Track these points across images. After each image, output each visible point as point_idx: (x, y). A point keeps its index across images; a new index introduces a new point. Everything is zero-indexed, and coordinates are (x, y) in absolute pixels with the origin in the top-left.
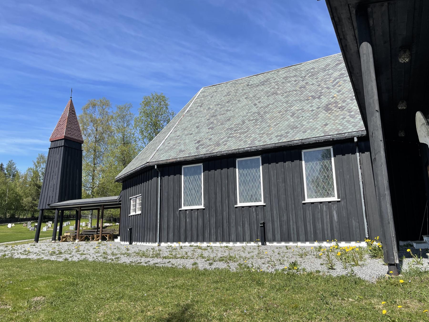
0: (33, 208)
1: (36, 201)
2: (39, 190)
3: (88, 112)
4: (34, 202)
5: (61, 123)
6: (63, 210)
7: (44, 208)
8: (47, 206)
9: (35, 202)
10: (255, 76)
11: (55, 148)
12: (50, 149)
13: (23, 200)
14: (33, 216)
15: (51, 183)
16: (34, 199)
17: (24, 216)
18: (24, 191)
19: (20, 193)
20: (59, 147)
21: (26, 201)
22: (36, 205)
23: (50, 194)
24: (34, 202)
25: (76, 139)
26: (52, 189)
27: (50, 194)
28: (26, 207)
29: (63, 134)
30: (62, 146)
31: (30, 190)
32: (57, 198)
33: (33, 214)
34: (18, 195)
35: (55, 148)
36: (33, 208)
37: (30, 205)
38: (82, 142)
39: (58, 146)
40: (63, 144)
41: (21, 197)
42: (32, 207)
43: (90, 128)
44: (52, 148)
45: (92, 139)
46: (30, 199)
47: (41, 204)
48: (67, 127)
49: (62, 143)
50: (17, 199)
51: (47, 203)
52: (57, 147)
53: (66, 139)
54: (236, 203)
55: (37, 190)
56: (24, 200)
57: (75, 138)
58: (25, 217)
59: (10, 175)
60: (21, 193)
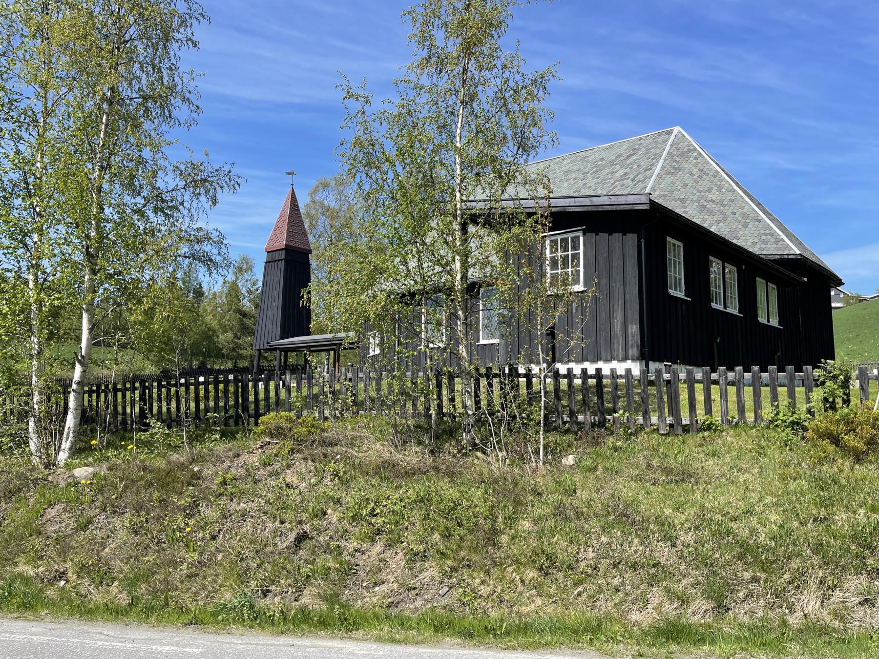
0: (235, 351)
1: (239, 339)
2: (243, 321)
3: (317, 198)
4: (236, 340)
5: (280, 225)
6: (287, 351)
7: (261, 348)
8: (266, 344)
9: (240, 341)
10: (535, 165)
11: (272, 262)
12: (266, 263)
13: (218, 337)
14: (235, 366)
15: (269, 311)
16: (236, 336)
17: (221, 365)
18: (219, 321)
19: (213, 325)
20: (279, 260)
21: (224, 338)
22: (239, 347)
23: (269, 327)
24: (236, 340)
25: (301, 248)
26: (271, 321)
27: (269, 327)
28: (225, 350)
29: (282, 242)
30: (282, 260)
31: (229, 320)
32: (278, 333)
33: (236, 362)
34: (209, 329)
35: (272, 262)
36: (235, 351)
37: (231, 346)
38: (310, 252)
39: (277, 259)
40: (283, 257)
41: (214, 332)
42: (234, 350)
43: (323, 222)
44: (269, 262)
45: (324, 242)
46: (230, 335)
47: (249, 347)
48: (288, 232)
49: (283, 255)
50: (209, 335)
51: (266, 341)
52: (275, 261)
53: (288, 249)
54: (478, 340)
55: (241, 320)
56: (221, 337)
57: (300, 246)
58: (222, 368)
59: (189, 292)
60: (214, 324)
